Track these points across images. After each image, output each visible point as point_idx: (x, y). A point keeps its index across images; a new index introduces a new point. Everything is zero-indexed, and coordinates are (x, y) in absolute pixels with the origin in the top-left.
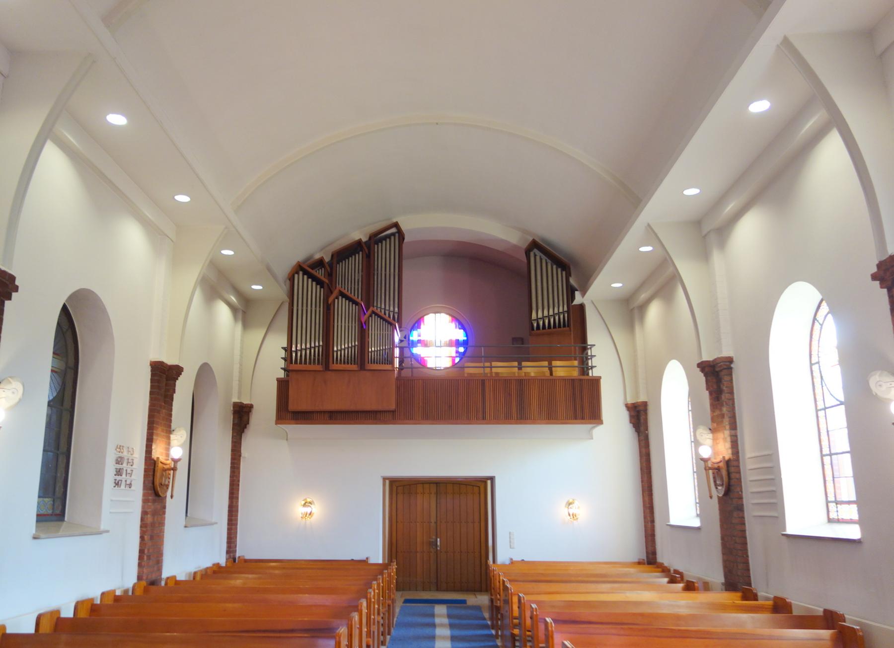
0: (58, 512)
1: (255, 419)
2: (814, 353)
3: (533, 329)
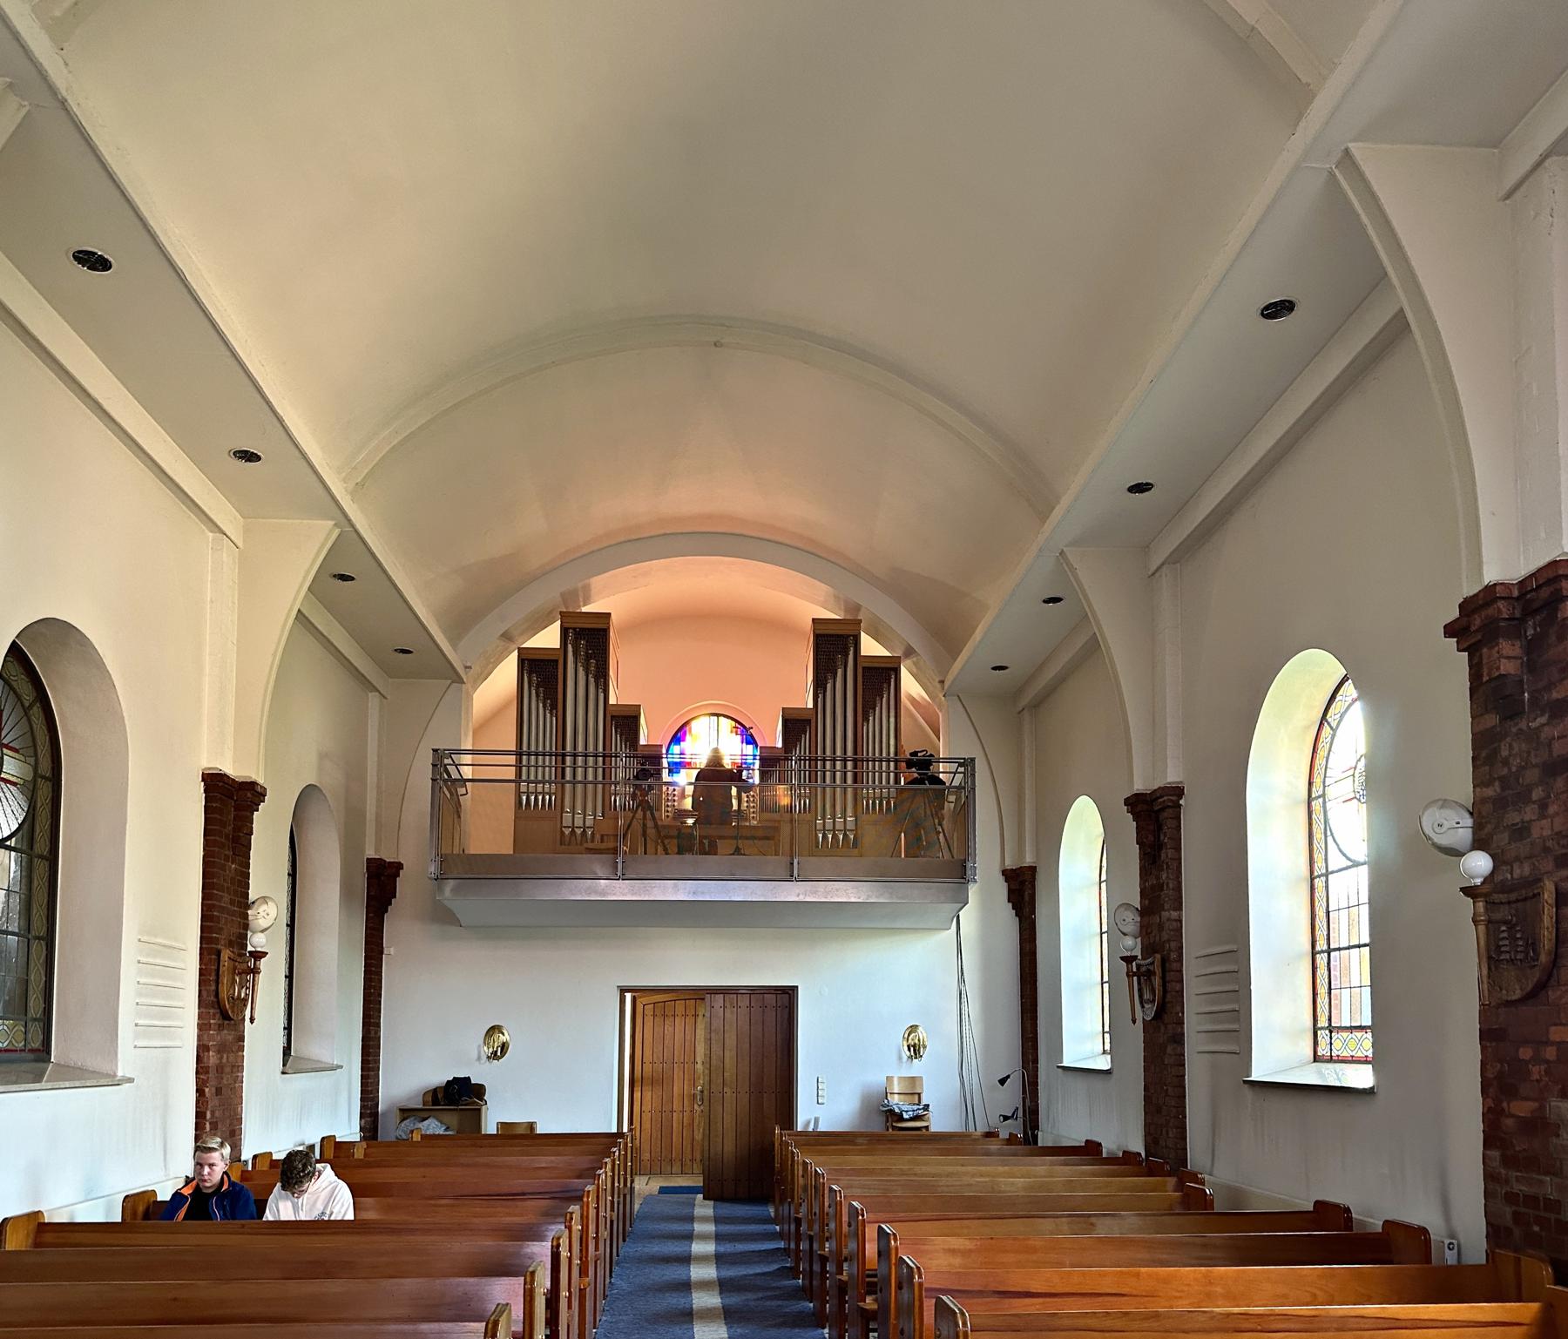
0: (37, 1045)
1: (405, 885)
2: (1318, 780)
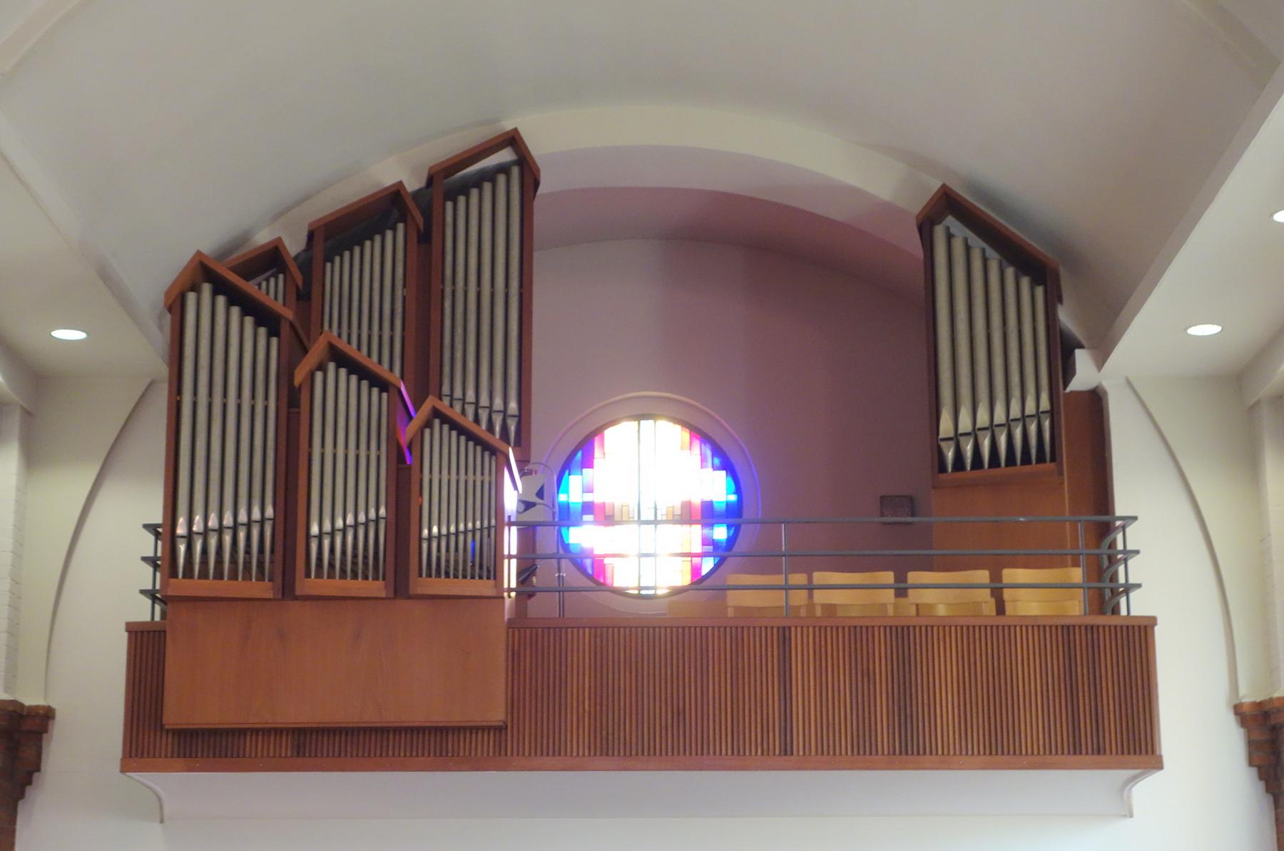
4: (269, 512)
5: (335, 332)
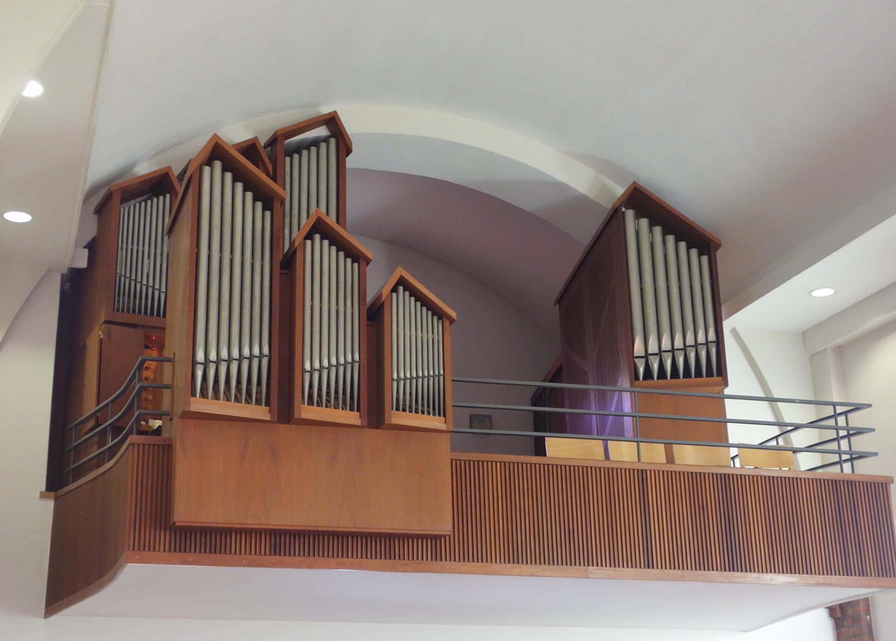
3: (637, 377)
4: (266, 350)
5: (323, 209)
